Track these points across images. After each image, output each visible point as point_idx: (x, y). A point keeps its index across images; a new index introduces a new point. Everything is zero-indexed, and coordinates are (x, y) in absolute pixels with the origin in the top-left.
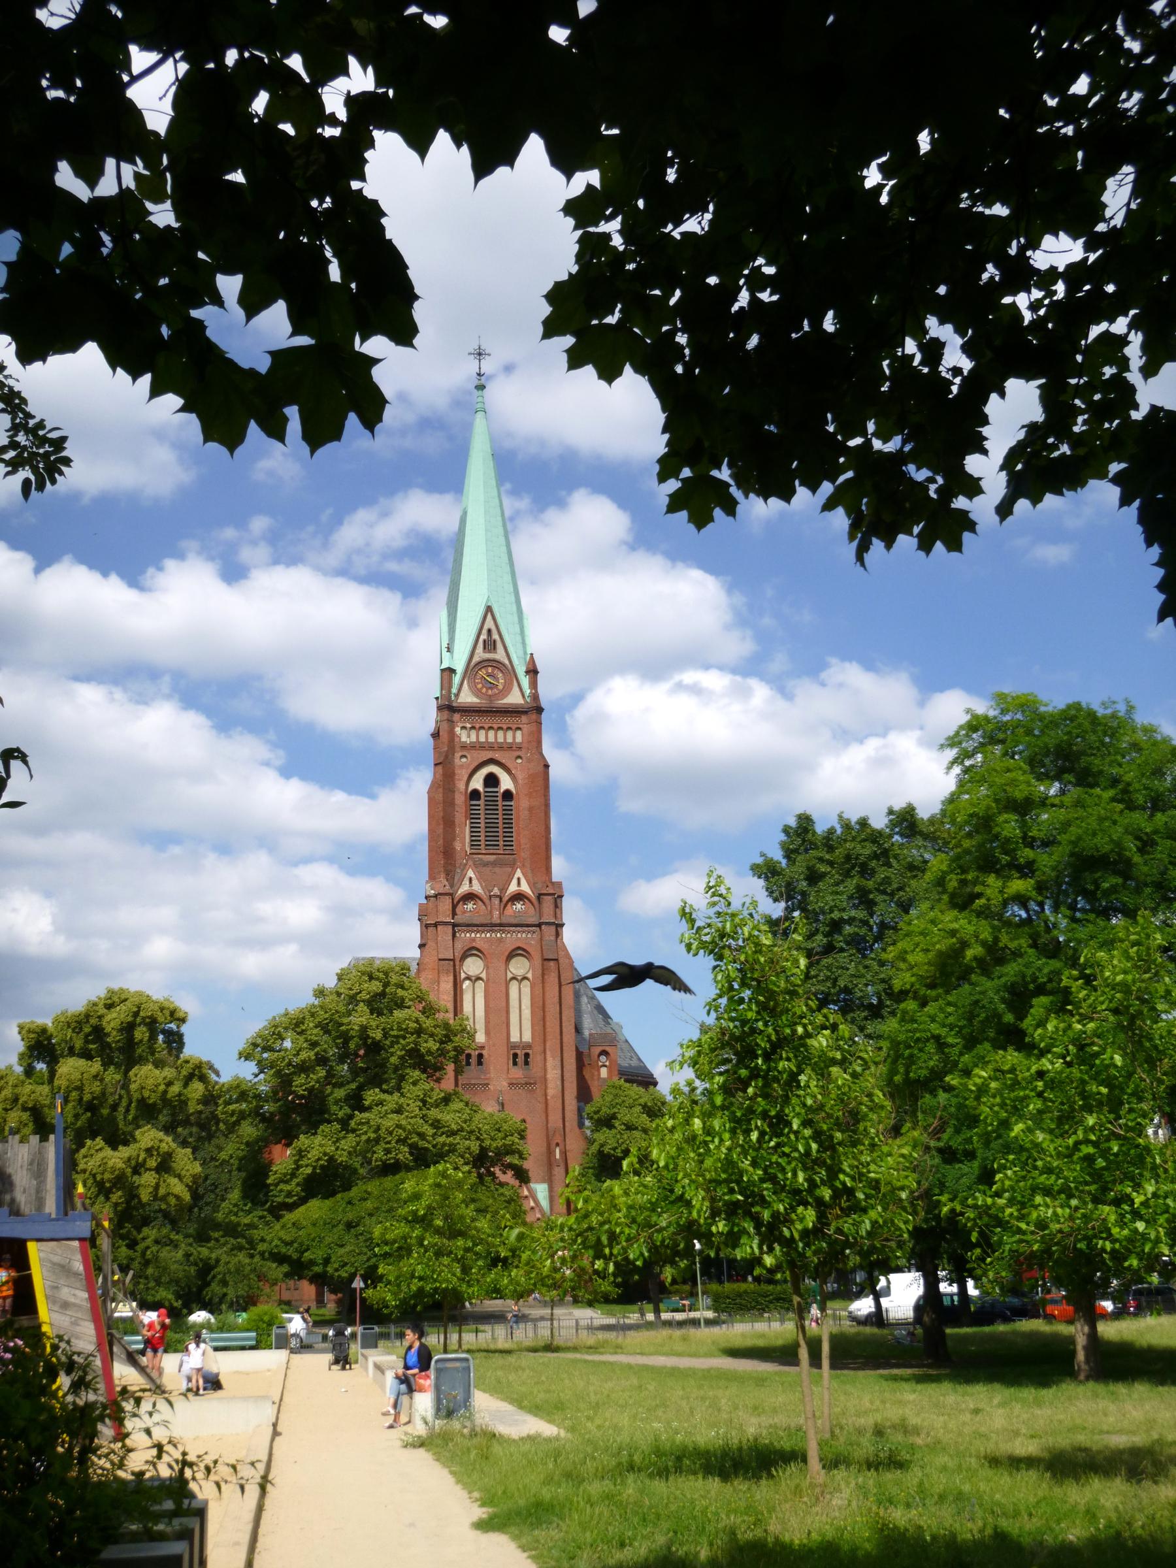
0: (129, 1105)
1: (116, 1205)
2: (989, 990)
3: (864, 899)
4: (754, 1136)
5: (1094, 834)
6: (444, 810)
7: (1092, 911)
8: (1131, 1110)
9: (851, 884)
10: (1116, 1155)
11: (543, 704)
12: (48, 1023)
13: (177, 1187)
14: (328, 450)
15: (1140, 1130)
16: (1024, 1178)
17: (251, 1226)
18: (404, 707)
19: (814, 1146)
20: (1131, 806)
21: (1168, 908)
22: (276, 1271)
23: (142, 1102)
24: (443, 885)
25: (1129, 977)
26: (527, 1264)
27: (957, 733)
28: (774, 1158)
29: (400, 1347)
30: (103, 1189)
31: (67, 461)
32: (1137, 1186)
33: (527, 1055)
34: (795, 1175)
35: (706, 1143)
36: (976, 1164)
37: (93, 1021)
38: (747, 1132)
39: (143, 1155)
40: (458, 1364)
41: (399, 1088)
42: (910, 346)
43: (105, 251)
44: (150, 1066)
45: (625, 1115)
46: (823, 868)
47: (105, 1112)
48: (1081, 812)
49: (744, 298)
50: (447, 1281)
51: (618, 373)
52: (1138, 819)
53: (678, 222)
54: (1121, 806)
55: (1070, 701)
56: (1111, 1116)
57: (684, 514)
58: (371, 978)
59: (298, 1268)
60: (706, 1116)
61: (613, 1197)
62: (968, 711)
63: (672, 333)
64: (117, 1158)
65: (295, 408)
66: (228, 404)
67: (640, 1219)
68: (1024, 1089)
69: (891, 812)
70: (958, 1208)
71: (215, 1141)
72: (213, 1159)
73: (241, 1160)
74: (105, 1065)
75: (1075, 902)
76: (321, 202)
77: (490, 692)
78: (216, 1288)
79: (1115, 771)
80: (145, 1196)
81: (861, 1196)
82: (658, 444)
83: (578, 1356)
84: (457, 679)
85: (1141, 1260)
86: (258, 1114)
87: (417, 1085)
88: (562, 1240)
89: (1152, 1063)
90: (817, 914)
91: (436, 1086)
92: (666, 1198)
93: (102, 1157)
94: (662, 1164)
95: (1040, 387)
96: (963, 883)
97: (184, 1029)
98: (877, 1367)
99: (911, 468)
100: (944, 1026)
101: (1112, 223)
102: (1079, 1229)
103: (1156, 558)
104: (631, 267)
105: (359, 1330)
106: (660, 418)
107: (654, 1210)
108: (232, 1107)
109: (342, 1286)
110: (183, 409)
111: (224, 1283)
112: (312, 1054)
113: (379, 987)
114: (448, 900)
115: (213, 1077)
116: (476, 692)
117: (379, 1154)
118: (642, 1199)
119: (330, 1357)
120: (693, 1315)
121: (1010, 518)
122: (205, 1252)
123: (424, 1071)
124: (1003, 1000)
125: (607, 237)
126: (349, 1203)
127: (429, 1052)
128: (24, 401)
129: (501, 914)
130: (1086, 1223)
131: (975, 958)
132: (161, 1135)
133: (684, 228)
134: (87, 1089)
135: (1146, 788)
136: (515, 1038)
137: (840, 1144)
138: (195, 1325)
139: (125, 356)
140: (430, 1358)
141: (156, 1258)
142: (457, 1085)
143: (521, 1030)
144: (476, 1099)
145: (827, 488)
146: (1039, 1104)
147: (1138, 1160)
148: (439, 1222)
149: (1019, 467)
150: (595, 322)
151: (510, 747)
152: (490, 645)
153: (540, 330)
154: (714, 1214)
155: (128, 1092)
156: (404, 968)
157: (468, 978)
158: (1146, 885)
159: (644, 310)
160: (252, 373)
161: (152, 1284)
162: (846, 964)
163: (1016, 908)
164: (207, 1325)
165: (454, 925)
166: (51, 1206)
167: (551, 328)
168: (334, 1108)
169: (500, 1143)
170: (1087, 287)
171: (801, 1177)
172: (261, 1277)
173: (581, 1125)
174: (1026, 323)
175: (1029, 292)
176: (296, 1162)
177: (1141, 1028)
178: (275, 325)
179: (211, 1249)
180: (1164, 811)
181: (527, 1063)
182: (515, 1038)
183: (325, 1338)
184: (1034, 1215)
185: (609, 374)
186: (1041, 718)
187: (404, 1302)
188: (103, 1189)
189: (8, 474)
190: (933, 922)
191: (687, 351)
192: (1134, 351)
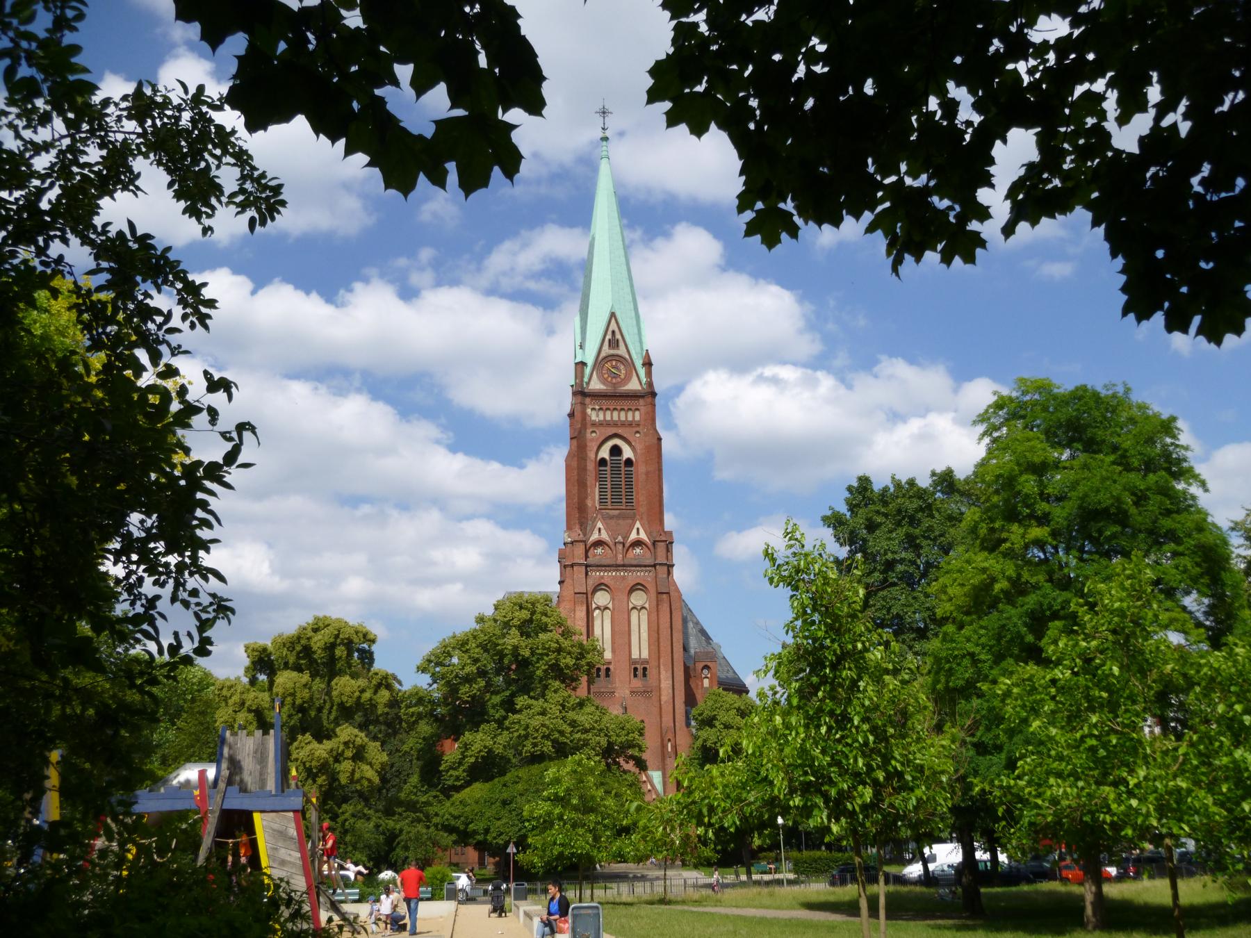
0: (331, 708)
1: (321, 786)
2: (1014, 616)
3: (911, 543)
4: (823, 730)
5: (1098, 491)
6: (578, 474)
7: (1096, 553)
8: (1127, 711)
9: (901, 532)
10: (1115, 746)
11: (657, 390)
12: (268, 643)
13: (369, 773)
14: (479, 194)
15: (1134, 727)
16: (1040, 765)
17: (427, 803)
18: (545, 395)
19: (871, 738)
20: (1128, 468)
21: (1159, 550)
22: (447, 839)
23: (341, 705)
24: (577, 534)
25: (1125, 605)
26: (644, 829)
27: (987, 411)
28: (840, 747)
29: (544, 899)
30: (310, 774)
31: (283, 203)
32: (1132, 772)
33: (645, 669)
34: (856, 761)
35: (785, 736)
36: (1003, 756)
37: (303, 642)
38: (818, 727)
39: (341, 747)
40: (590, 911)
41: (543, 695)
42: (933, 103)
43: (311, 47)
44: (348, 677)
45: (723, 717)
46: (879, 519)
47: (313, 713)
48: (1087, 474)
49: (801, 71)
50: (582, 848)
51: (706, 129)
52: (1134, 478)
53: (750, 14)
54: (1120, 468)
55: (1078, 384)
56: (1111, 716)
57: (758, 237)
58: (521, 608)
59: (464, 837)
60: (786, 714)
61: (712, 778)
62: (995, 393)
63: (746, 99)
64: (321, 750)
65: (454, 164)
66: (402, 160)
67: (733, 795)
68: (1040, 693)
69: (933, 474)
70: (987, 788)
71: (399, 736)
72: (398, 750)
73: (419, 751)
74: (313, 676)
75: (1083, 546)
76: (472, 8)
78: (399, 852)
79: (1115, 440)
80: (343, 779)
81: (908, 778)
82: (737, 185)
83: (686, 908)
84: (588, 371)
85: (1134, 830)
86: (432, 715)
87: (557, 693)
88: (671, 811)
89: (1143, 673)
90: (875, 556)
91: (573, 693)
92: (754, 779)
93: (310, 749)
94: (750, 751)
95: (1036, 134)
96: (992, 530)
97: (374, 648)
98: (925, 918)
99: (935, 199)
100: (977, 645)
101: (1092, 6)
102: (1085, 805)
103: (1120, 267)
104: (715, 48)
105: (512, 886)
106: (738, 164)
107: (744, 789)
108: (411, 710)
109: (500, 851)
110: (369, 165)
111: (406, 848)
112: (474, 669)
113: (527, 615)
114: (582, 546)
115: (397, 686)
116: (604, 381)
117: (528, 746)
118: (734, 779)
119: (489, 907)
120: (777, 876)
121: (1012, 237)
122: (391, 823)
123: (563, 682)
124: (1025, 624)
125: (696, 25)
126: (504, 785)
127: (567, 667)
128: (250, 157)
129: (624, 557)
130: (1090, 801)
131: (1002, 590)
132: (356, 731)
133: (754, 17)
134: (298, 695)
135: (1140, 454)
136: (635, 655)
137: (892, 736)
138: (383, 881)
139: (325, 125)
140: (568, 906)
141: (353, 828)
142: (589, 692)
143: (640, 649)
144: (605, 704)
145: (868, 217)
146: (1052, 706)
147: (1132, 750)
148: (575, 802)
149: (1021, 196)
150: (687, 90)
151: (630, 425)
152: (614, 343)
153: (645, 97)
154: (792, 791)
155: (331, 698)
156: (547, 600)
157: (598, 608)
158: (1140, 531)
159: (722, 79)
160: (420, 137)
161: (350, 848)
162: (898, 597)
163: (1035, 551)
164: (394, 881)
165: (587, 566)
166: (271, 785)
167: (654, 96)
168: (492, 711)
169: (623, 739)
170: (1073, 56)
171: (860, 762)
172: (435, 843)
173: (688, 725)
174: (1025, 84)
175: (1027, 61)
176: (462, 753)
177: (1135, 646)
178: (438, 101)
179: (397, 821)
180: (1155, 472)
181: (645, 675)
182: (635, 655)
183: (486, 892)
184: (1049, 793)
185: (699, 130)
186: (1055, 398)
187: (548, 863)
188: (311, 774)
189: (238, 213)
190: (968, 562)
191: (758, 112)
192: (1111, 105)
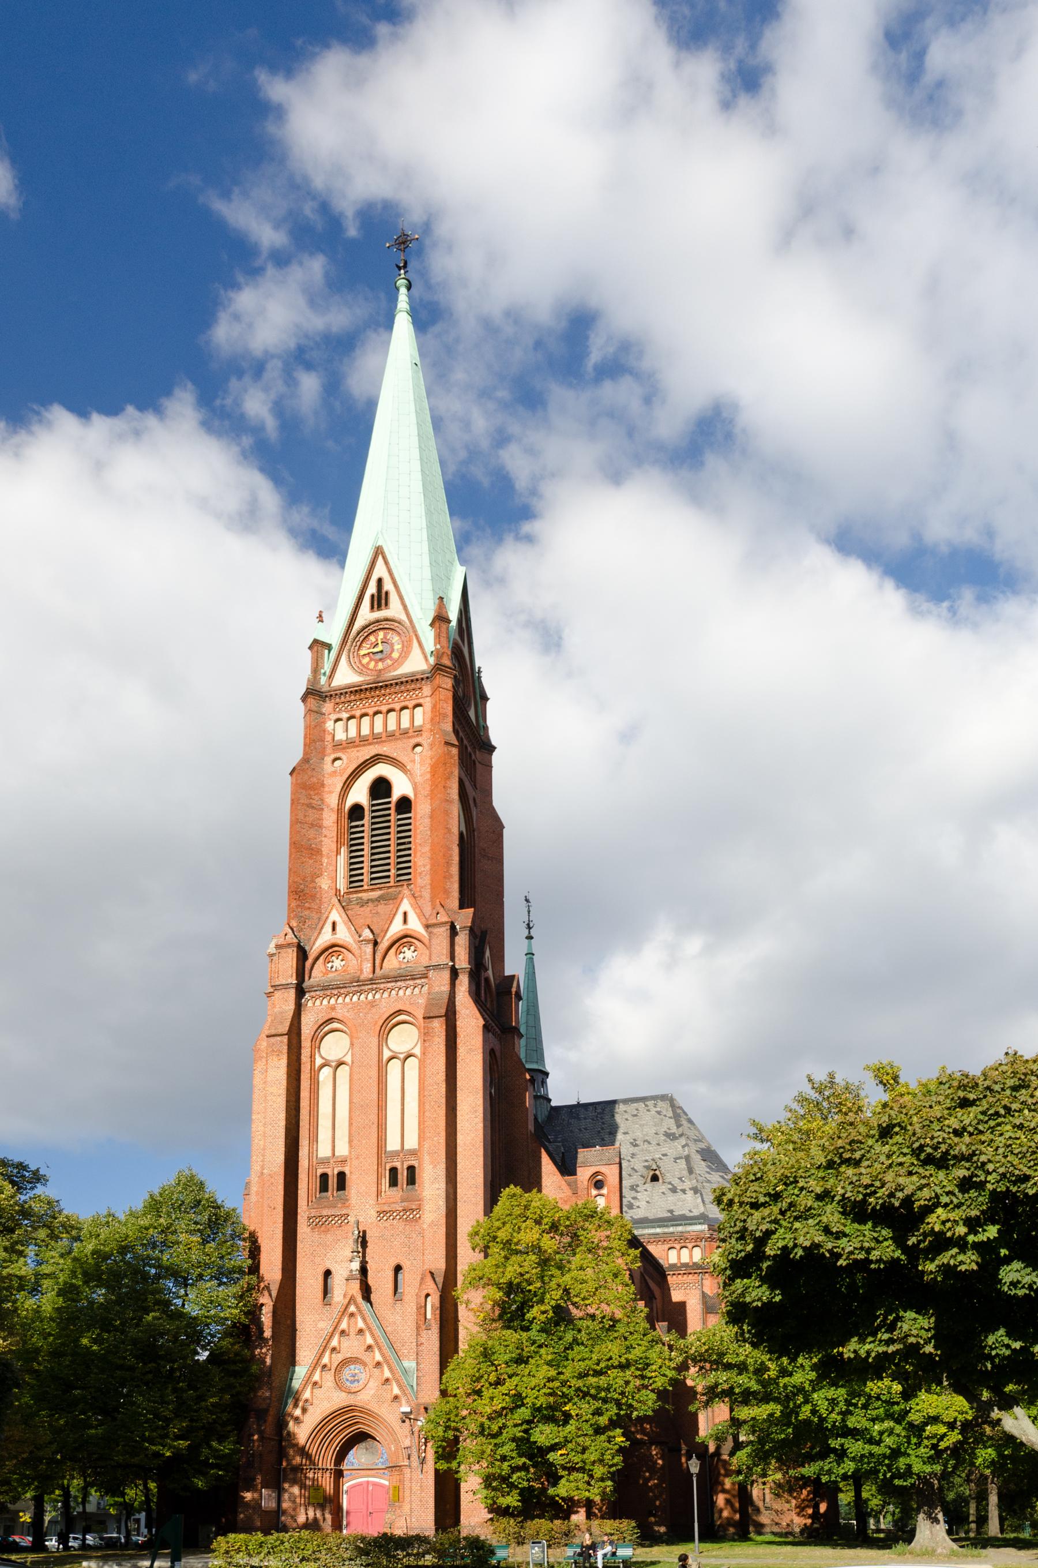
77: (380, 666)
116: (361, 670)
136: (393, 1144)
152: (380, 600)
